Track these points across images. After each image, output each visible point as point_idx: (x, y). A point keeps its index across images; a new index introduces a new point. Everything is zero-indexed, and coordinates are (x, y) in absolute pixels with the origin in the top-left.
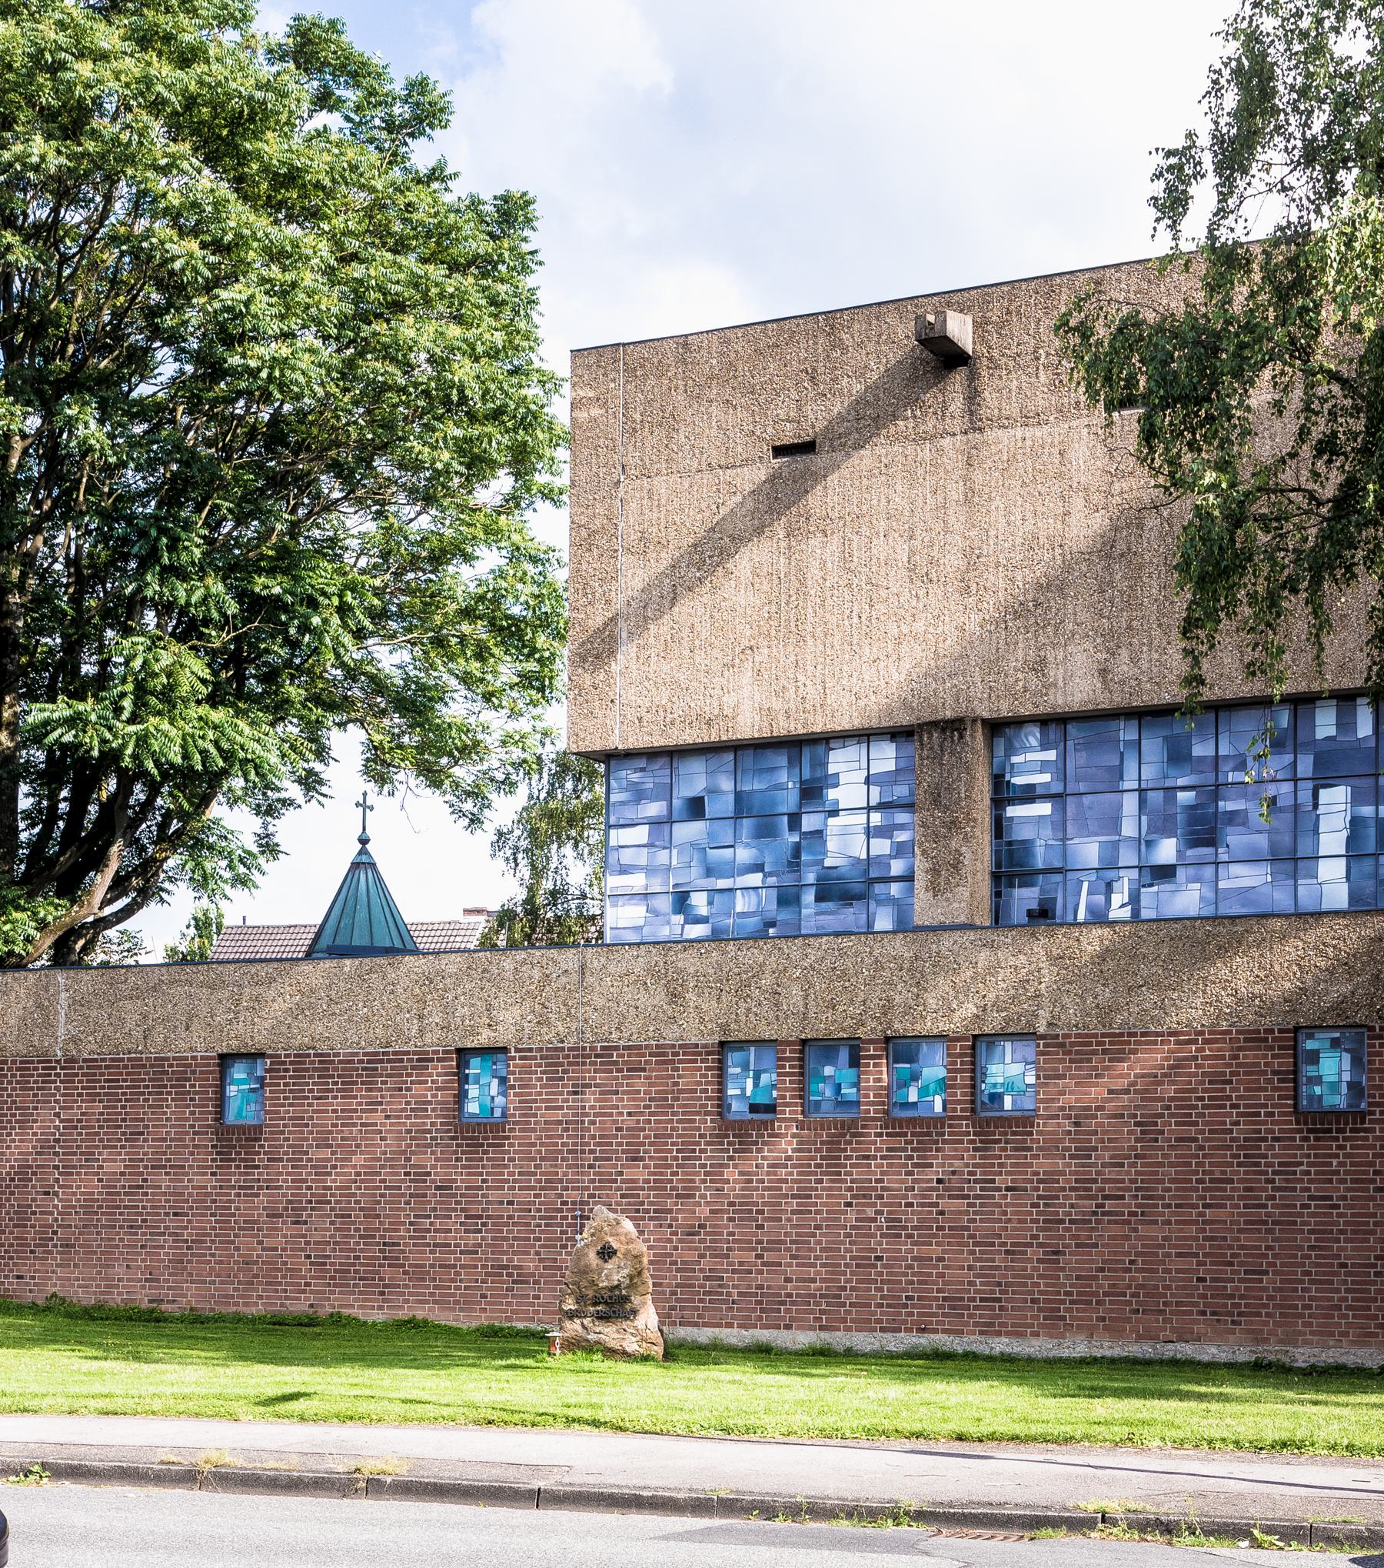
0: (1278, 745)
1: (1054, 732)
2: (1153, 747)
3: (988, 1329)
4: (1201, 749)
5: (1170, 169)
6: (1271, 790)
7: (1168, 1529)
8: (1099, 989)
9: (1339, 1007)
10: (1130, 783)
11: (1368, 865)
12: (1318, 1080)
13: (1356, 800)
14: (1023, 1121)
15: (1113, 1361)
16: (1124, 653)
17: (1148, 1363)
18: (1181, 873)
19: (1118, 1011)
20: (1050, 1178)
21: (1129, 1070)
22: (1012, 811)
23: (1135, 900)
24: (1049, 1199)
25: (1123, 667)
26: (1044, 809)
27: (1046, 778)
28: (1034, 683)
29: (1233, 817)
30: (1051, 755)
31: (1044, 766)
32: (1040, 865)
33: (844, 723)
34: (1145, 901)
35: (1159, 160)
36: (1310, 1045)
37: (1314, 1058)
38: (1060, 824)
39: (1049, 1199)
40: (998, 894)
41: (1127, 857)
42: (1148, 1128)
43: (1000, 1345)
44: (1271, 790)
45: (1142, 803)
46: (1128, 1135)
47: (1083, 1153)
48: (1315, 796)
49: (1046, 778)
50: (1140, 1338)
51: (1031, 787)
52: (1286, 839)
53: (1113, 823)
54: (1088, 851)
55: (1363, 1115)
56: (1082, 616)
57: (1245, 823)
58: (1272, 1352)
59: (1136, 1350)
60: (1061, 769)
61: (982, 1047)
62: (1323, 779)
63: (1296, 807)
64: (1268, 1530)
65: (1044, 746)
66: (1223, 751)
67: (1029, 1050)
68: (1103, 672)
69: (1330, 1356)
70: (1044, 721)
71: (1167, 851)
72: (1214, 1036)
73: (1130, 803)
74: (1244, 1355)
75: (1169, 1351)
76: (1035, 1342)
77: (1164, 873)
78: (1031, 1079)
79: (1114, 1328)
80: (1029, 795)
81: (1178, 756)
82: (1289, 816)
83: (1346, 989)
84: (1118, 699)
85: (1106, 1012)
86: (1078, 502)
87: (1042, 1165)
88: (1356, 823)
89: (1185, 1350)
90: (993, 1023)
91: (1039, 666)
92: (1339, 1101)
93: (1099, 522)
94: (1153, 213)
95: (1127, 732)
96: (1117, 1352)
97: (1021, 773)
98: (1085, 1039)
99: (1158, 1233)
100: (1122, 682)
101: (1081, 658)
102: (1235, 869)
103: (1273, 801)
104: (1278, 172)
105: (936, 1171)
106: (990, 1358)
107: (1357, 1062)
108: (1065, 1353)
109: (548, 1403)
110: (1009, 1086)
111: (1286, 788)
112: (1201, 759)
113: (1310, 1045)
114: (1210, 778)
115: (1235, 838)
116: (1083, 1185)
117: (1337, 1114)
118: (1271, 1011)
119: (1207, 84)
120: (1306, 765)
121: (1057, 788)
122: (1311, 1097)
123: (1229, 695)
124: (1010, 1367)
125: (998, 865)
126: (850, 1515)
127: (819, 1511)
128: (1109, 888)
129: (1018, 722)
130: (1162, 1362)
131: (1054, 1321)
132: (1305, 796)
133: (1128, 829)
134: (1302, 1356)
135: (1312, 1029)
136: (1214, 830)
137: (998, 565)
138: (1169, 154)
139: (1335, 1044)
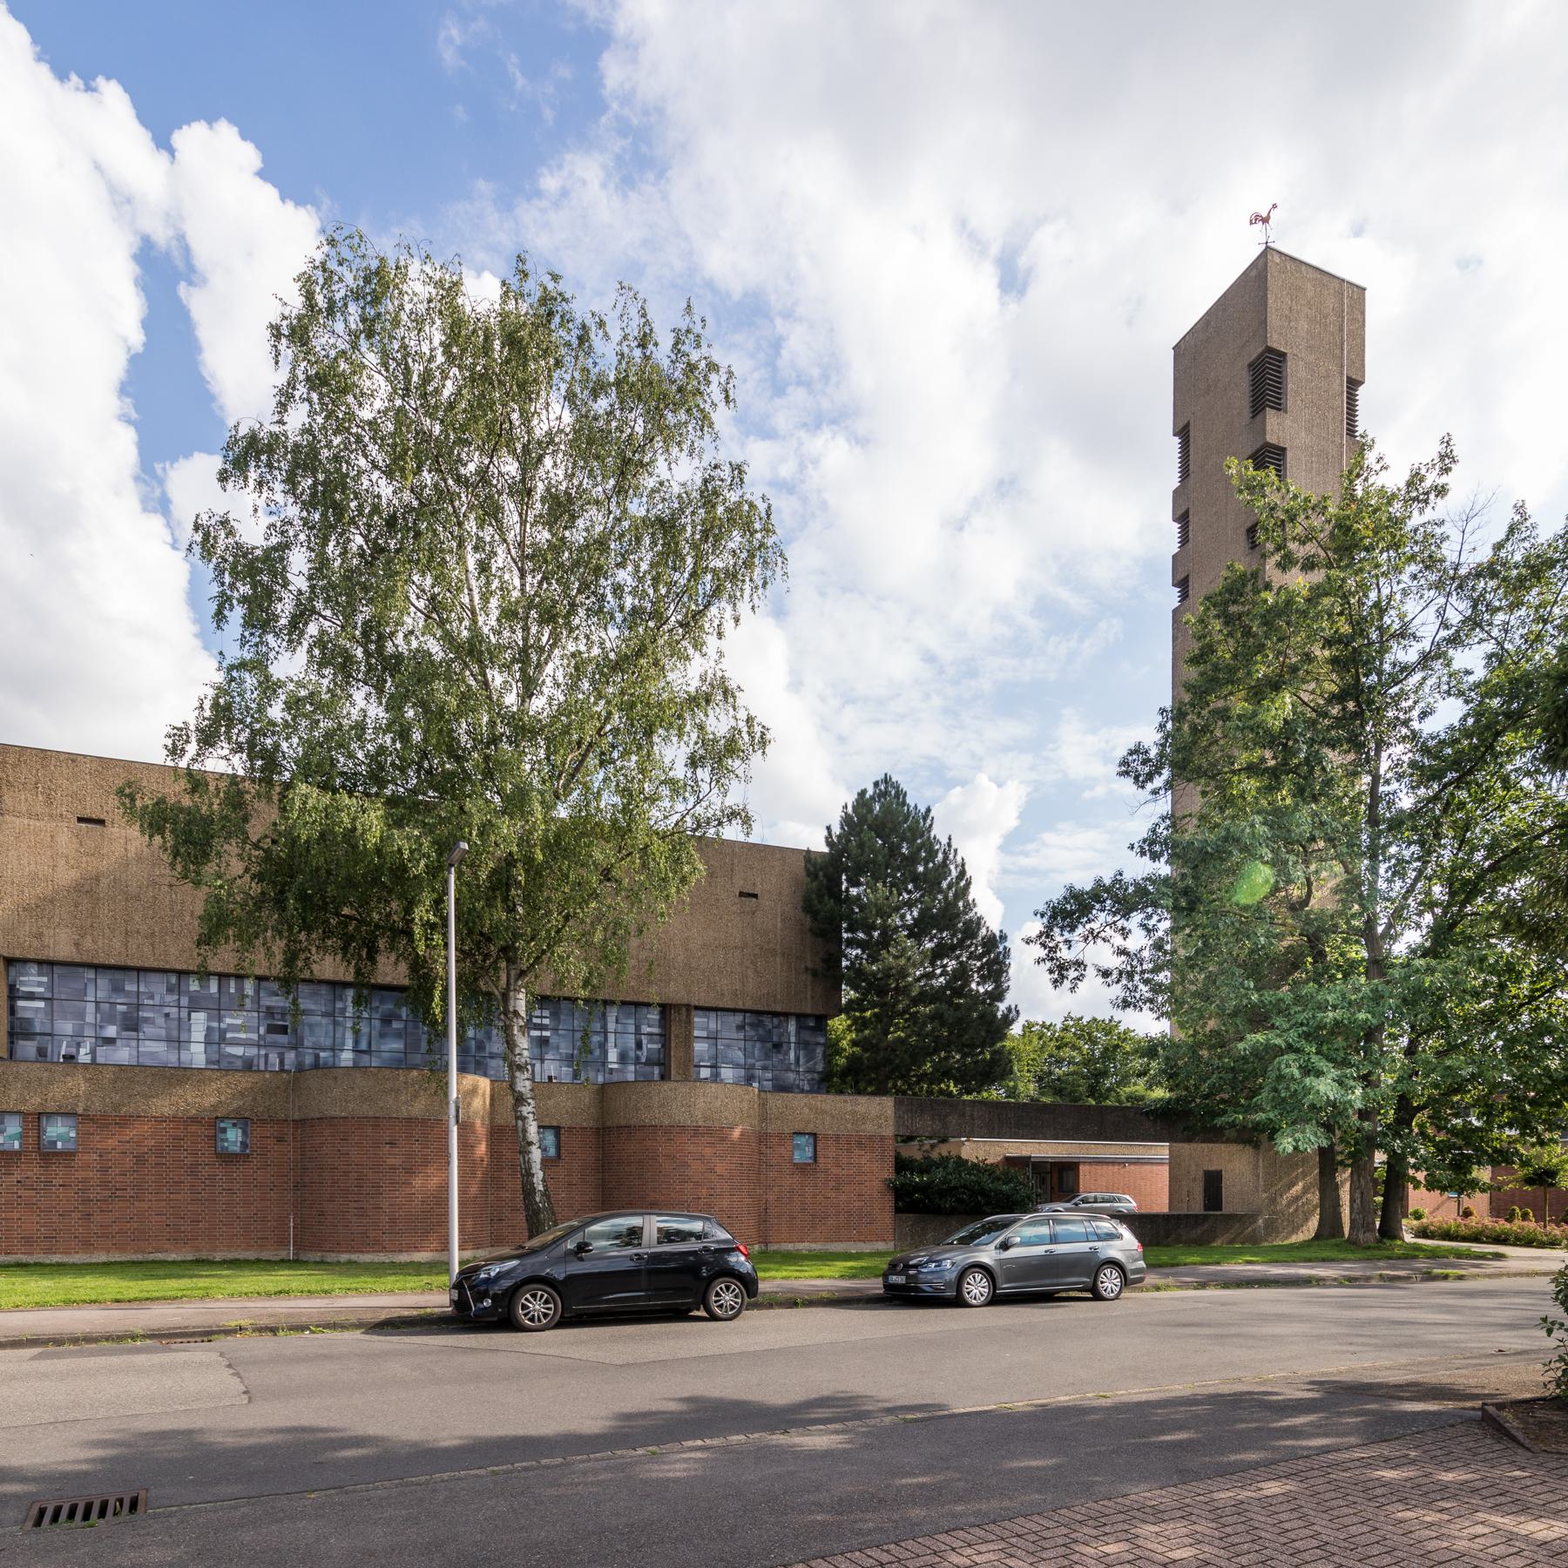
0: (170, 990)
1: (45, 968)
2: (104, 982)
3: (48, 1251)
4: (130, 987)
5: (175, 735)
6: (167, 1010)
7: (273, 1330)
8: (113, 1095)
9: (237, 1110)
10: (91, 998)
11: (215, 1047)
12: (227, 1140)
13: (209, 1019)
14: (67, 1155)
15: (121, 1263)
16: (89, 938)
17: (140, 1263)
18: (119, 1042)
19: (124, 1105)
20: (85, 1180)
21: (131, 1133)
22: (20, 1003)
23: (93, 1052)
24: (84, 1191)
25: (88, 943)
26: (41, 1004)
27: (42, 990)
28: (36, 943)
29: (146, 1020)
30: (45, 979)
31: (40, 984)
32: (38, 1030)
33: (32, 956)
34: (98, 1053)
35: (169, 729)
36: (222, 1125)
37: (224, 1130)
38: (50, 1013)
39: (84, 1191)
40: (12, 1043)
41: (89, 1032)
42: (140, 1160)
43: (56, 1258)
44: (167, 1010)
45: (97, 1009)
46: (129, 1161)
47: (104, 1170)
48: (189, 1015)
49: (42, 990)
50: (135, 1252)
51: (33, 993)
52: (175, 1033)
53: (81, 1015)
54: (66, 1027)
55: (248, 1156)
56: (64, 916)
57: (153, 1023)
58: (204, 1255)
59: (134, 1257)
60: (51, 986)
61: (44, 1120)
62: (193, 1008)
63: (179, 1019)
64: (318, 1326)
65: (40, 974)
66: (141, 989)
67: (71, 1121)
68: (77, 945)
69: (230, 1256)
70: (40, 963)
71: (111, 1031)
72: (174, 1119)
73: (91, 1008)
74: (190, 1257)
75: (151, 1257)
76: (77, 1256)
77: (110, 1041)
78: (73, 1134)
79: (121, 1248)
80: (31, 997)
81: (117, 989)
82: (176, 1023)
83: (241, 1103)
84: (85, 959)
85: (117, 1107)
86: (62, 862)
87: (81, 1175)
88: (209, 1029)
89: (160, 1256)
90: (51, 1106)
91: (39, 936)
92: (236, 1149)
93: (74, 874)
94: (166, 752)
95: (90, 974)
96: (123, 1258)
97: (25, 986)
98: (105, 1116)
99: (145, 1205)
100: (88, 951)
101: (64, 936)
102: (147, 1043)
103: (167, 1015)
104: (226, 752)
105: (17, 1176)
106: (51, 1265)
107: (245, 1133)
108: (94, 1261)
109: (1545, 1263)
110: (60, 1137)
111: (175, 1010)
112: (129, 992)
113: (222, 1125)
114: (135, 1001)
115: (148, 1030)
116: (104, 1184)
117: (236, 1155)
118: (204, 1110)
119: (198, 705)
120: (185, 1001)
121: (49, 995)
122: (223, 1147)
123: (146, 965)
124: (105, 1268)
125: (12, 1028)
126: (107, 1339)
127: (89, 1339)
128: (78, 1045)
129: (25, 961)
130: (147, 1262)
131: (87, 1245)
132: (184, 1014)
133: (90, 1018)
134: (218, 1257)
135: (223, 1119)
136: (137, 1025)
137: (13, 883)
138: (174, 728)
139: (234, 1125)
